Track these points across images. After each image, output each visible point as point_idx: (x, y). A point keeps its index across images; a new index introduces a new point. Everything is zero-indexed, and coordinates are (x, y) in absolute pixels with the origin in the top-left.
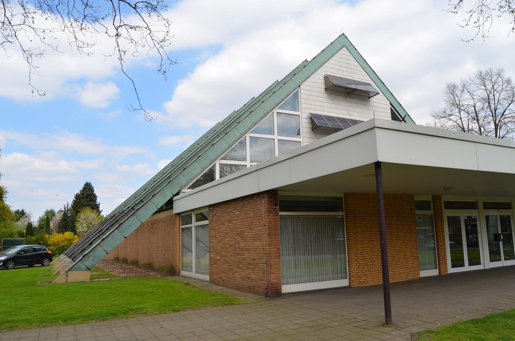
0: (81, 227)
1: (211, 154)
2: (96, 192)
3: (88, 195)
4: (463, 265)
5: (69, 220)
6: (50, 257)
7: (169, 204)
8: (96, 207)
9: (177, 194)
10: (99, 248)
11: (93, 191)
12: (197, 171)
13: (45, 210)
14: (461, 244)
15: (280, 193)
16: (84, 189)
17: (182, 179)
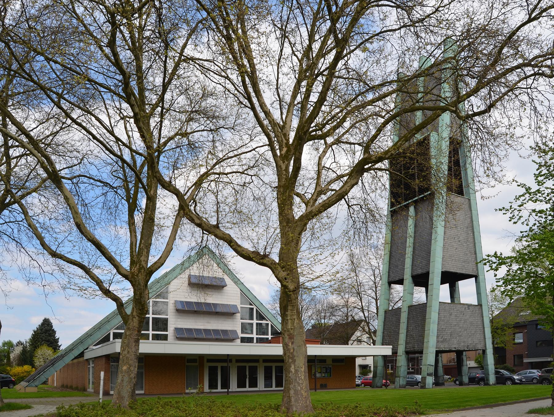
0: (39, 362)
1: (108, 327)
2: (55, 327)
3: (47, 331)
4: (245, 387)
5: (28, 355)
6: (14, 383)
7: (82, 355)
8: (53, 343)
9: (87, 349)
10: (42, 376)
11: (52, 326)
12: (100, 336)
13: (2, 341)
14: (271, 378)
15: (111, 356)
16: (43, 324)
17: (90, 341)
